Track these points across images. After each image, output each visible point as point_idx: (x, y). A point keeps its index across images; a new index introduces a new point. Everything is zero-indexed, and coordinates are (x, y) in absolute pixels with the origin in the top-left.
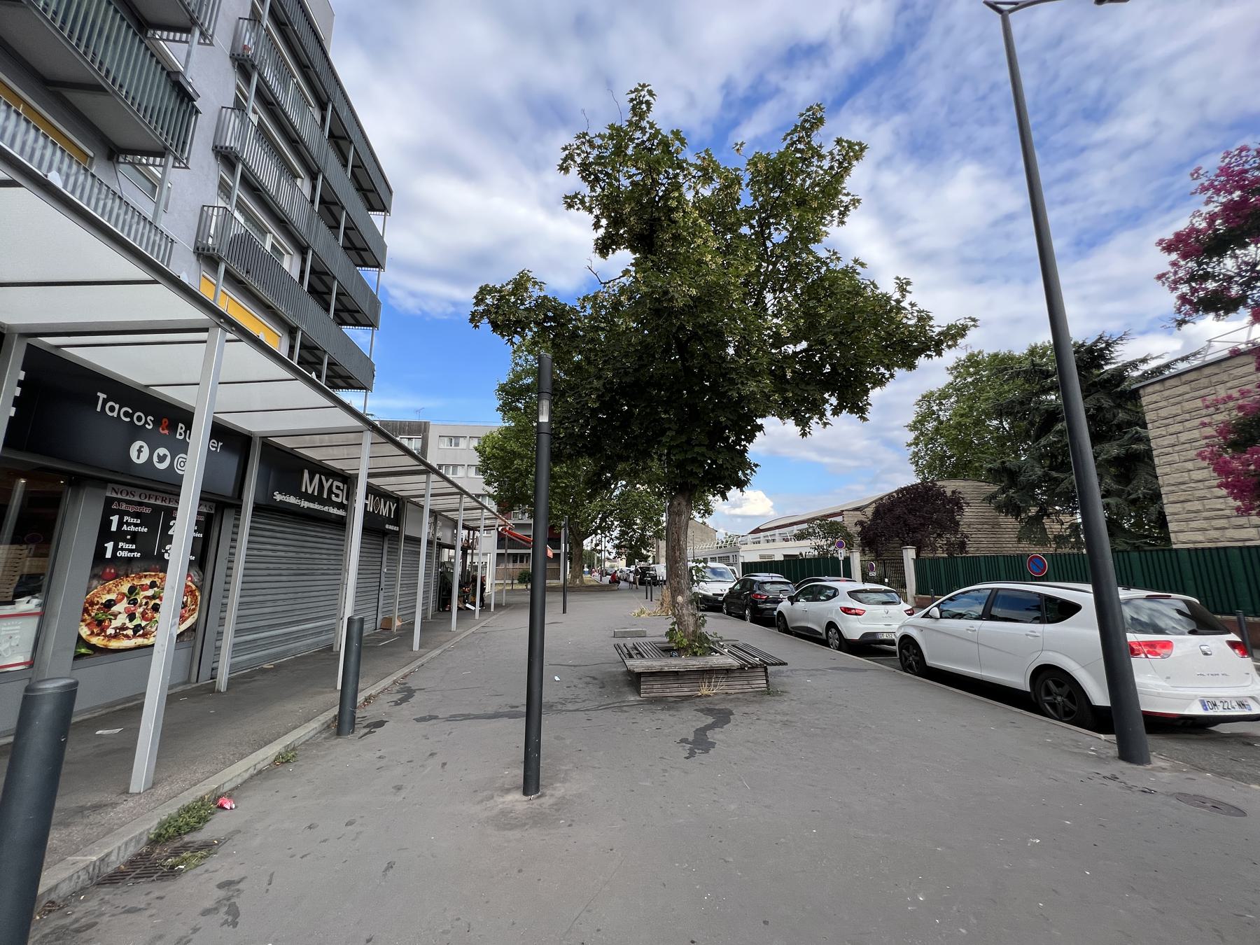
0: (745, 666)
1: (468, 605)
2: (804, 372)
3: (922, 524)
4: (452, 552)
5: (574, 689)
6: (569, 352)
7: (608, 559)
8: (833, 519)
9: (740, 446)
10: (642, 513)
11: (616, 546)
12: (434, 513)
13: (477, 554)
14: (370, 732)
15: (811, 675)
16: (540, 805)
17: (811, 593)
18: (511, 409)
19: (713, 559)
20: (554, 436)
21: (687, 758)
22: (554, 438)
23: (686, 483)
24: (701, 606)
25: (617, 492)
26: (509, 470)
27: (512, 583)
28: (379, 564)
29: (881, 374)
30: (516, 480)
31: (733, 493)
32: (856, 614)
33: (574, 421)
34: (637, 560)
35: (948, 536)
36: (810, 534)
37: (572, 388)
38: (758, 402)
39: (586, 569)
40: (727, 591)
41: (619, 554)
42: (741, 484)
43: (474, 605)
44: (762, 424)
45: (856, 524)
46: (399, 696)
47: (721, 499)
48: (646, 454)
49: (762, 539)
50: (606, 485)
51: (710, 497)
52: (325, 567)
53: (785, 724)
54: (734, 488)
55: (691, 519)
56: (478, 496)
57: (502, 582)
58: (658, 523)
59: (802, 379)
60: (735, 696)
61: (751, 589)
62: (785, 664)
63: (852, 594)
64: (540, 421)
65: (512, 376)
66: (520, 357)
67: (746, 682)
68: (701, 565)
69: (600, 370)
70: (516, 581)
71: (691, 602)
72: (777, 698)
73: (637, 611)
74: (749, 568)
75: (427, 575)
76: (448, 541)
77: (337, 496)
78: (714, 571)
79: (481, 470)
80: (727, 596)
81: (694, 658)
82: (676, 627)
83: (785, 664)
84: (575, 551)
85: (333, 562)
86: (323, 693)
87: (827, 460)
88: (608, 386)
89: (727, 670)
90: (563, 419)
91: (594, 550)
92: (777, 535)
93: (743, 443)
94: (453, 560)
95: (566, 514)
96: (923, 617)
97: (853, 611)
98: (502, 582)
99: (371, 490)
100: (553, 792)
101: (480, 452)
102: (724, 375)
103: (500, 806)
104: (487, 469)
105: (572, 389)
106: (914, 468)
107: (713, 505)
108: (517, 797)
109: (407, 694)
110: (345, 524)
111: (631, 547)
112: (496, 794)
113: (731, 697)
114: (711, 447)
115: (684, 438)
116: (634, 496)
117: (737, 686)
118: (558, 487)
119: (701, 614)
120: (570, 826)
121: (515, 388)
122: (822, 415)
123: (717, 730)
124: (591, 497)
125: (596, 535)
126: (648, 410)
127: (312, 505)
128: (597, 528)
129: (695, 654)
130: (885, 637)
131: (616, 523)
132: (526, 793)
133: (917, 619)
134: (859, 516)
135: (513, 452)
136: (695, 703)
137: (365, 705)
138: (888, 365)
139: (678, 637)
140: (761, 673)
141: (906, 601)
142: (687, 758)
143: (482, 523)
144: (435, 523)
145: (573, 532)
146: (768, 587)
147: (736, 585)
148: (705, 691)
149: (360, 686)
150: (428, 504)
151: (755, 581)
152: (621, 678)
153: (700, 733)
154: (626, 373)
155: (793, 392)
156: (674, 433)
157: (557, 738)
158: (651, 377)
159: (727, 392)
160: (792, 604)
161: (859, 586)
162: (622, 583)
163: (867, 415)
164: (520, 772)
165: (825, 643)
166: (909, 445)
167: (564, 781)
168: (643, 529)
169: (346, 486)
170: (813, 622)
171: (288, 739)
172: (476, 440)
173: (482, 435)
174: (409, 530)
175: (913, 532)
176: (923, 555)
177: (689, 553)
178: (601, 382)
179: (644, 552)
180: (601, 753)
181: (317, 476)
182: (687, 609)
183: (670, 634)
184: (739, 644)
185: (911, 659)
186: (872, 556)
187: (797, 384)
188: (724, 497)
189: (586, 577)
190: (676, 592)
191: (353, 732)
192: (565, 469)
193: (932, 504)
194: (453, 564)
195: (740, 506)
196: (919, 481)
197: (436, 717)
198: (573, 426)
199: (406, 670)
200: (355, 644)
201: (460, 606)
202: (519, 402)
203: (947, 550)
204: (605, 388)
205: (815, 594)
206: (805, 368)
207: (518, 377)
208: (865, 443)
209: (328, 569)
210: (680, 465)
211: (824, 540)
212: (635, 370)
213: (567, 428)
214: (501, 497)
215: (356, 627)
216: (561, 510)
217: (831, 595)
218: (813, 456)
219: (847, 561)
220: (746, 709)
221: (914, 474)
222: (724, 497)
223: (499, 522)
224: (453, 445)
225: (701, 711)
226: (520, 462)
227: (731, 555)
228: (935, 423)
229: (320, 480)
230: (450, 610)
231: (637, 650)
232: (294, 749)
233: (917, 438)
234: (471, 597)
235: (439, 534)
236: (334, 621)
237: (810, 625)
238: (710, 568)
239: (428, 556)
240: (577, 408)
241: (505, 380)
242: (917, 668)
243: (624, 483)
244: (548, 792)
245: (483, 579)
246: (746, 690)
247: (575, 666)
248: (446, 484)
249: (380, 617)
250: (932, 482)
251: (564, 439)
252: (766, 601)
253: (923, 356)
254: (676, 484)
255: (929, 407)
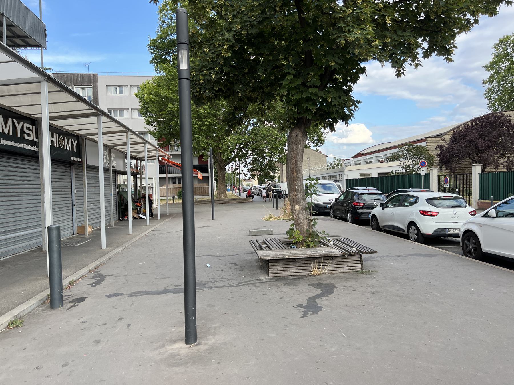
0: (345, 254)
1: (141, 216)
2: (402, 20)
3: (490, 147)
4: (125, 177)
5: (220, 272)
6: (204, 8)
7: (245, 180)
8: (419, 144)
9: (346, 86)
10: (270, 144)
11: (250, 170)
12: (106, 146)
13: (144, 178)
14: (75, 305)
15: (395, 260)
16: (198, 351)
17: (398, 201)
18: (162, 61)
19: (324, 178)
20: (194, 83)
21: (302, 317)
22: (196, 84)
23: (302, 118)
24: (313, 212)
25: (250, 128)
26: (164, 112)
27: (174, 199)
28: (70, 187)
29: (467, 19)
30: (171, 120)
31: (340, 125)
32: (431, 215)
33: (211, 69)
34: (266, 180)
35: (509, 155)
36: (399, 156)
37: (208, 40)
38: (361, 47)
39: (229, 188)
40: (334, 201)
41: (253, 176)
42: (345, 118)
43: (146, 216)
44: (364, 67)
45: (436, 148)
46: (94, 280)
47: (329, 130)
48: (270, 96)
49: (362, 162)
50: (240, 122)
51: (322, 130)
52: (28, 190)
53: (373, 293)
54: (340, 121)
55: (307, 147)
56: (142, 133)
57: (165, 198)
58: (282, 151)
59: (400, 27)
60: (338, 275)
61: (352, 199)
62: (375, 252)
63: (430, 201)
64: (181, 68)
65: (160, 33)
66: (166, 16)
67: (346, 265)
68: (313, 182)
69: (231, 23)
70: (176, 197)
71: (306, 209)
72: (369, 276)
73: (266, 217)
74: (351, 183)
75: (107, 194)
76: (120, 168)
77: (28, 135)
78: (324, 186)
79: (143, 112)
80: (334, 204)
81: (308, 249)
82: (294, 228)
83: (375, 252)
84: (220, 174)
85: (33, 186)
86: (38, 280)
87: (417, 97)
88: (238, 38)
89: (332, 257)
90: (202, 68)
91: (233, 173)
92: (374, 158)
93: (349, 84)
94: (126, 183)
95: (211, 146)
96: (483, 216)
97: (429, 213)
98: (165, 198)
99: (53, 130)
100: (207, 342)
101: (140, 98)
102: (334, 25)
103: (170, 352)
104: (147, 111)
105: (208, 41)
106: (487, 101)
107: (325, 136)
108: (182, 345)
109: (100, 279)
110: (38, 158)
111: (262, 170)
112: (167, 343)
113: (335, 275)
114: (323, 87)
115: (300, 81)
116: (263, 131)
117: (339, 268)
118: (204, 125)
119: (312, 217)
120: (219, 363)
121: (163, 44)
122: (415, 58)
123: (324, 298)
124: (228, 133)
125: (235, 162)
126: (271, 58)
127: (9, 143)
128: (235, 157)
129: (308, 246)
130: (452, 232)
131: (250, 152)
132: (187, 342)
133: (478, 218)
134: (439, 141)
135: (166, 97)
136: (308, 280)
137: (69, 288)
138: (474, 12)
139: (296, 235)
140: (357, 258)
141: (470, 205)
142: (302, 317)
143: (146, 155)
144: (109, 155)
145: (217, 160)
146: (365, 197)
147: (340, 196)
148: (315, 272)
149: (64, 274)
150: (101, 140)
151: (355, 193)
152: (255, 264)
153: (312, 300)
154: (252, 26)
155: (391, 38)
156: (292, 77)
157: (209, 305)
158: (273, 28)
159: (335, 39)
160: (383, 209)
161: (435, 194)
162: (256, 197)
163: (452, 57)
164: (183, 329)
165: (406, 237)
166: (485, 83)
167: (214, 334)
168: (270, 157)
169: (34, 127)
170: (399, 222)
171: (16, 312)
172: (136, 88)
173: (140, 84)
174: (89, 161)
175: (481, 153)
176: (487, 170)
177: (305, 174)
178: (232, 34)
179: (272, 174)
180: (241, 315)
181: (10, 120)
182: (303, 214)
183: (290, 232)
184: (341, 238)
185: (471, 247)
186: (448, 172)
187: (395, 32)
188: (332, 129)
189: (229, 193)
190: (294, 202)
191: (62, 306)
192: (208, 111)
193: (499, 130)
194: (126, 186)
195: (346, 137)
196: (490, 112)
197: (122, 294)
198: (210, 73)
199: (97, 263)
200: (55, 246)
201: (135, 216)
202: (168, 55)
203: (507, 166)
204: (235, 40)
205: (400, 202)
206: (403, 17)
207: (165, 34)
208: (449, 82)
209: (31, 192)
210: (298, 104)
211: (410, 161)
212: (260, 23)
213: (205, 75)
214: (159, 134)
215: (54, 233)
216: (207, 143)
217: (413, 202)
218: (406, 94)
219: (428, 176)
220: (345, 284)
221: (487, 106)
222: (332, 129)
223: (158, 153)
224: (118, 92)
225: (313, 285)
226: (172, 106)
227: (337, 174)
228: (508, 64)
229: (13, 123)
230: (128, 219)
231: (266, 244)
232: (21, 318)
233: (492, 77)
234: (143, 210)
235: (114, 163)
236: (40, 229)
237: (396, 224)
238: (320, 184)
239: (106, 180)
240: (212, 58)
241: (155, 37)
242: (475, 254)
243: (255, 120)
244: (203, 342)
245: (151, 197)
246: (346, 271)
247: (221, 256)
248: (113, 124)
249: (75, 225)
250: (500, 112)
251: (204, 85)
252: (364, 207)
253: (504, 2)
254: (295, 119)
255: (505, 50)
